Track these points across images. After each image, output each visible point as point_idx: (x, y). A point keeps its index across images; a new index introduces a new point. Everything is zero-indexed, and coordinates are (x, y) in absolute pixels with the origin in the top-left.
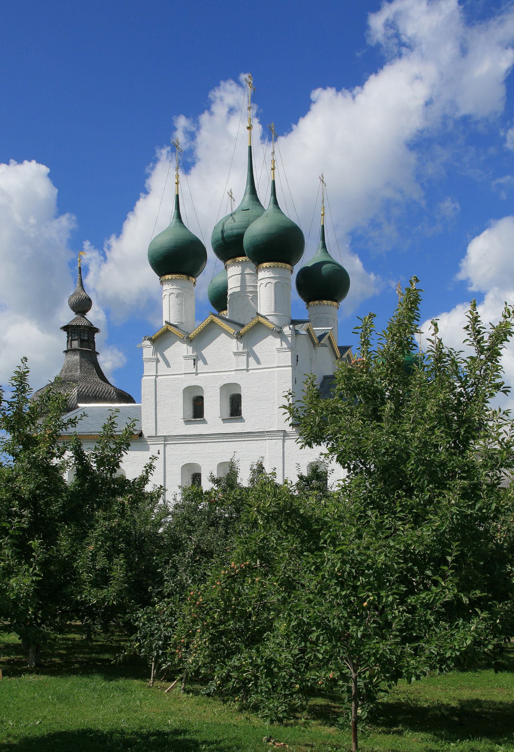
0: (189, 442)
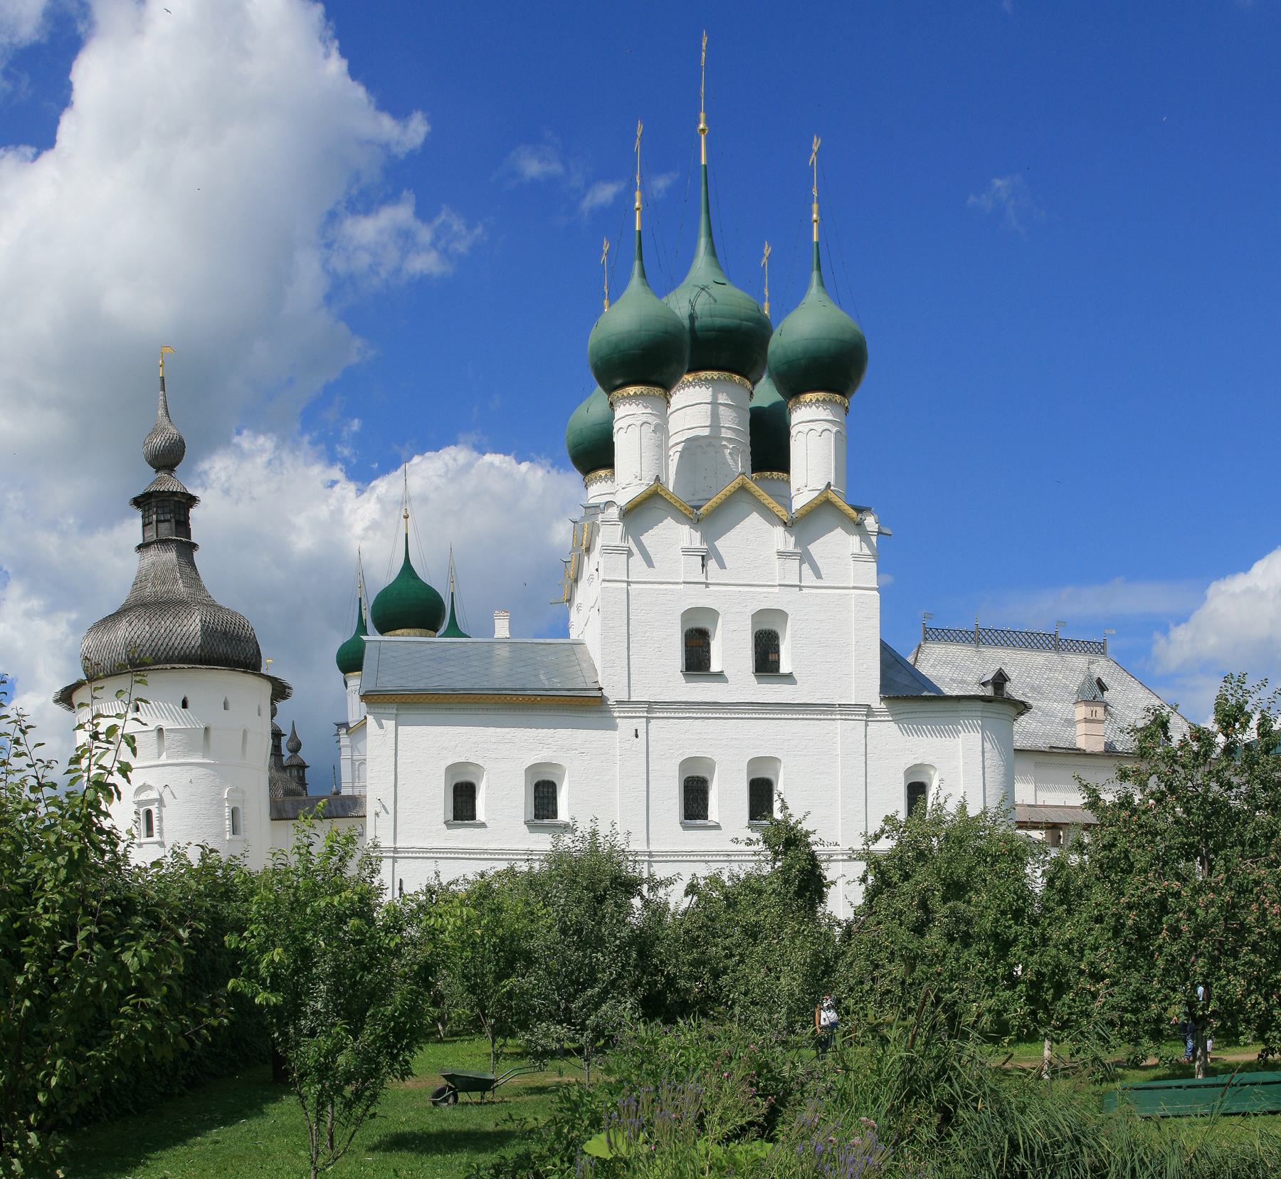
0: (695, 715)
